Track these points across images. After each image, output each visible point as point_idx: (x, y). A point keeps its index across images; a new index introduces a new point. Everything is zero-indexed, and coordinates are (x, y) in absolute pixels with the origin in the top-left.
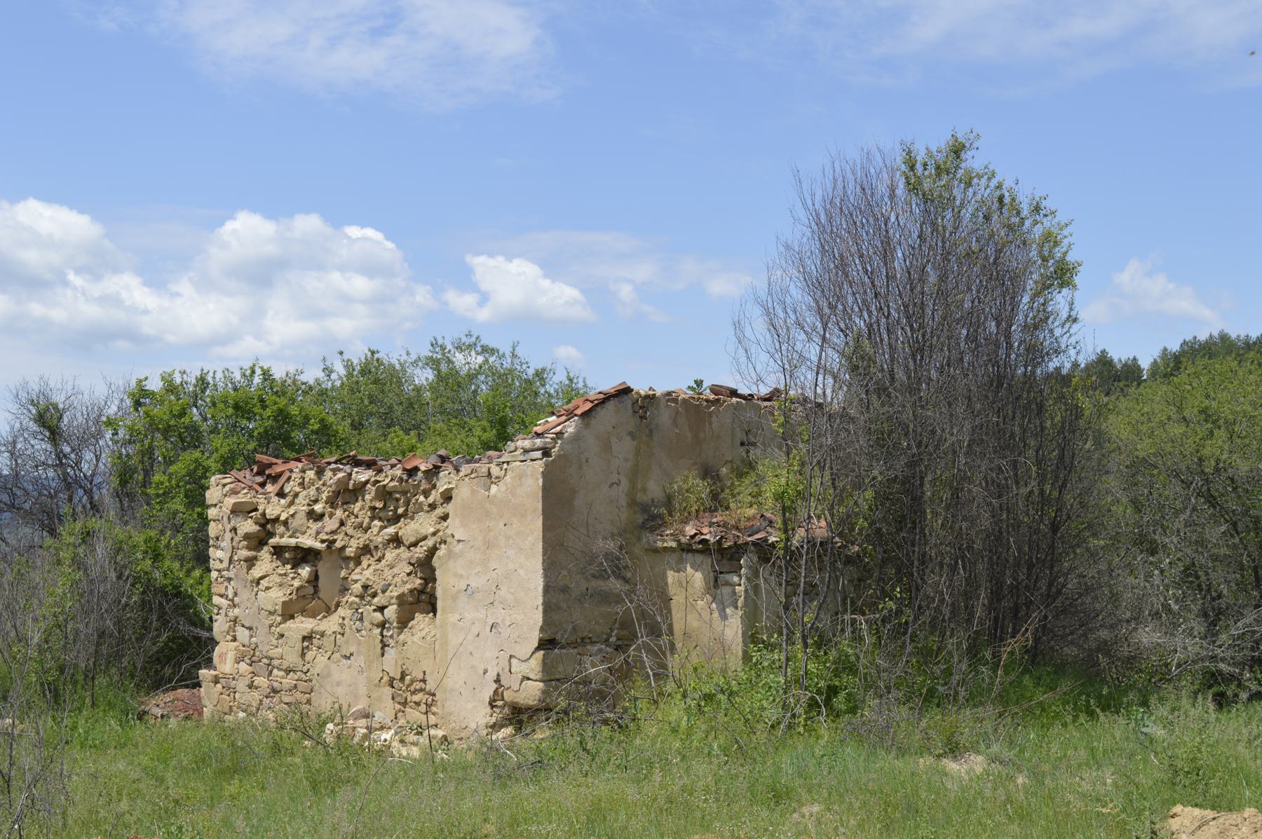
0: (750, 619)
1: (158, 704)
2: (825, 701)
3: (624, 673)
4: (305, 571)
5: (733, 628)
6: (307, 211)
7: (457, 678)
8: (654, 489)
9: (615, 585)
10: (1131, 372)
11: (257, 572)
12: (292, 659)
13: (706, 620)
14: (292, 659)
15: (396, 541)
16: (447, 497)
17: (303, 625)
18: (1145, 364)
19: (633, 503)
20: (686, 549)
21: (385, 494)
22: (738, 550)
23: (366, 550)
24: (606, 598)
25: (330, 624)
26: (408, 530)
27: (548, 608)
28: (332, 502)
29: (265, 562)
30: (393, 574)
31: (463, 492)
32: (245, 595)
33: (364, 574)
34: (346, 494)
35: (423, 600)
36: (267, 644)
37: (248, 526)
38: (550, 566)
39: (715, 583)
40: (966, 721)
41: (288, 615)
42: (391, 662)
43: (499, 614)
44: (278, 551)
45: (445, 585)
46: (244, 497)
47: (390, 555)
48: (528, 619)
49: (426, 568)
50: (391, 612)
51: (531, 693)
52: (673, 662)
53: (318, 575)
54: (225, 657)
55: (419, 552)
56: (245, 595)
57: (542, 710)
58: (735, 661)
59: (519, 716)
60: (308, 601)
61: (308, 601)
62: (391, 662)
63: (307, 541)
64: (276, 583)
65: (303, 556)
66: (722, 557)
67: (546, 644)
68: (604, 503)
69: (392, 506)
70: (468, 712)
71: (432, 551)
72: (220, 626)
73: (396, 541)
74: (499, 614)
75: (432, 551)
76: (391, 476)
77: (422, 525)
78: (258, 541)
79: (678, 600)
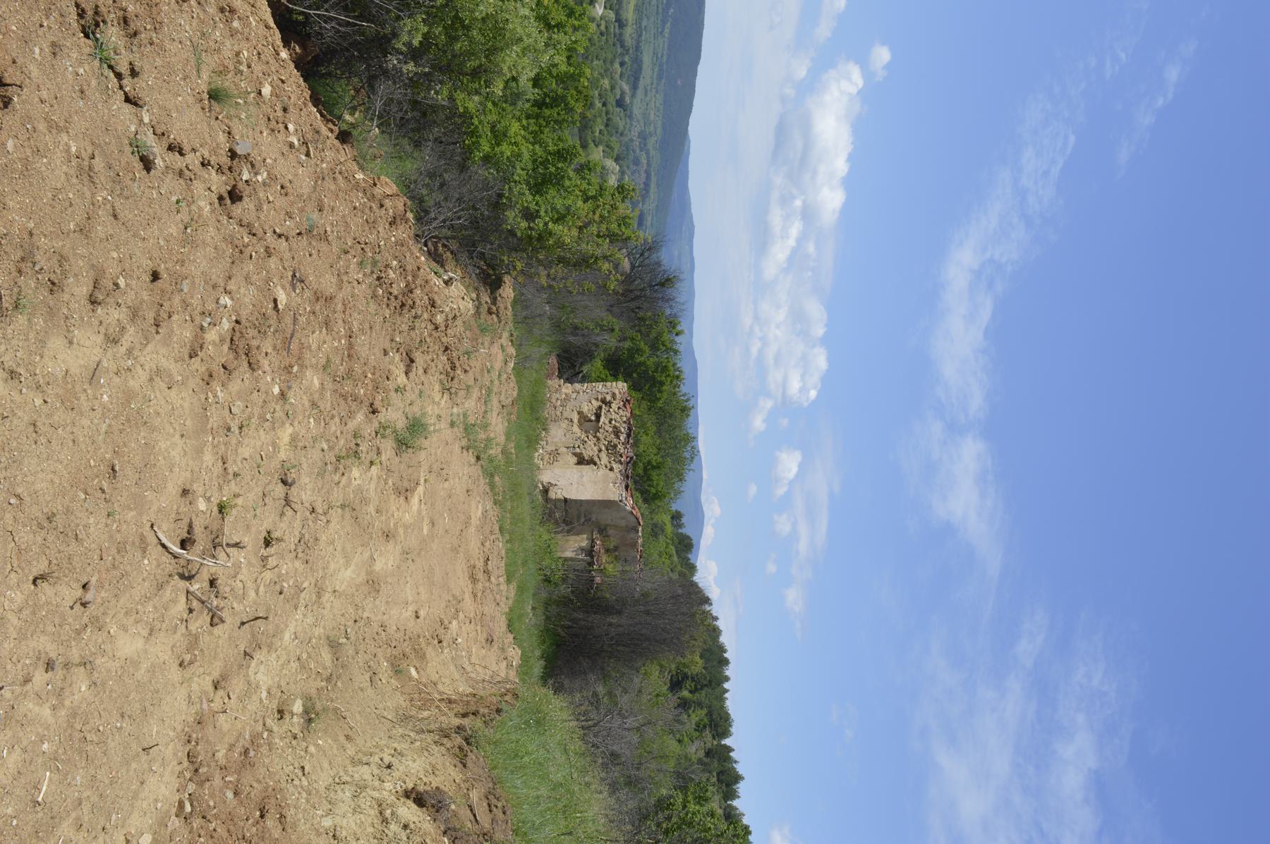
0: (571, 559)
1: (553, 360)
2: (547, 580)
3: (557, 523)
4: (593, 418)
5: (569, 554)
6: (829, 359)
7: (557, 471)
8: (611, 532)
9: (582, 520)
10: (730, 794)
11: (594, 402)
12: (565, 414)
13: (572, 546)
14: (565, 414)
15: (600, 451)
16: (611, 469)
17: (576, 417)
18: (735, 803)
19: (606, 526)
20: (593, 541)
21: (615, 446)
22: (592, 557)
23: (599, 439)
24: (579, 517)
25: (576, 429)
26: (603, 455)
27: (576, 501)
28: (615, 427)
29: (596, 404)
30: (590, 450)
31: (611, 474)
32: (586, 397)
33: (591, 442)
34: (617, 433)
35: (581, 461)
36: (570, 406)
37: (608, 398)
38: (588, 502)
39: (582, 549)
40: (540, 612)
41: (579, 413)
42: (563, 450)
43: (575, 486)
44: (600, 408)
45: (586, 469)
46: (618, 396)
47: (596, 449)
48: (573, 495)
49: (591, 462)
50: (578, 450)
51: (552, 495)
52: (559, 536)
53: (590, 423)
54: (567, 389)
55: (596, 459)
56: (586, 397)
57: (547, 500)
58: (559, 554)
59: (546, 491)
60: (583, 419)
61: (583, 419)
62: (563, 450)
63: (602, 419)
64: (589, 409)
65: (598, 416)
66: (590, 552)
67: (566, 500)
68: (606, 517)
69: (611, 448)
70: (545, 477)
71: (595, 464)
72: (577, 386)
73: (600, 451)
74: (575, 486)
75: (595, 464)
76: (620, 448)
77: (604, 459)
78: (604, 401)
79: (578, 538)
